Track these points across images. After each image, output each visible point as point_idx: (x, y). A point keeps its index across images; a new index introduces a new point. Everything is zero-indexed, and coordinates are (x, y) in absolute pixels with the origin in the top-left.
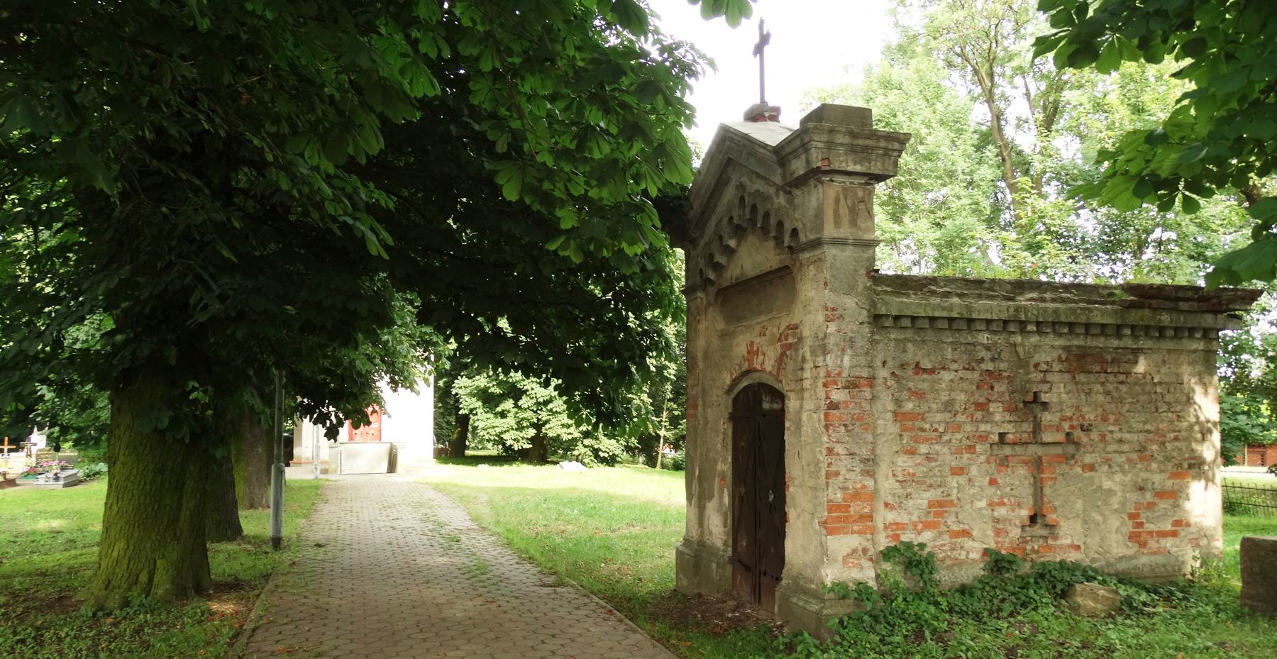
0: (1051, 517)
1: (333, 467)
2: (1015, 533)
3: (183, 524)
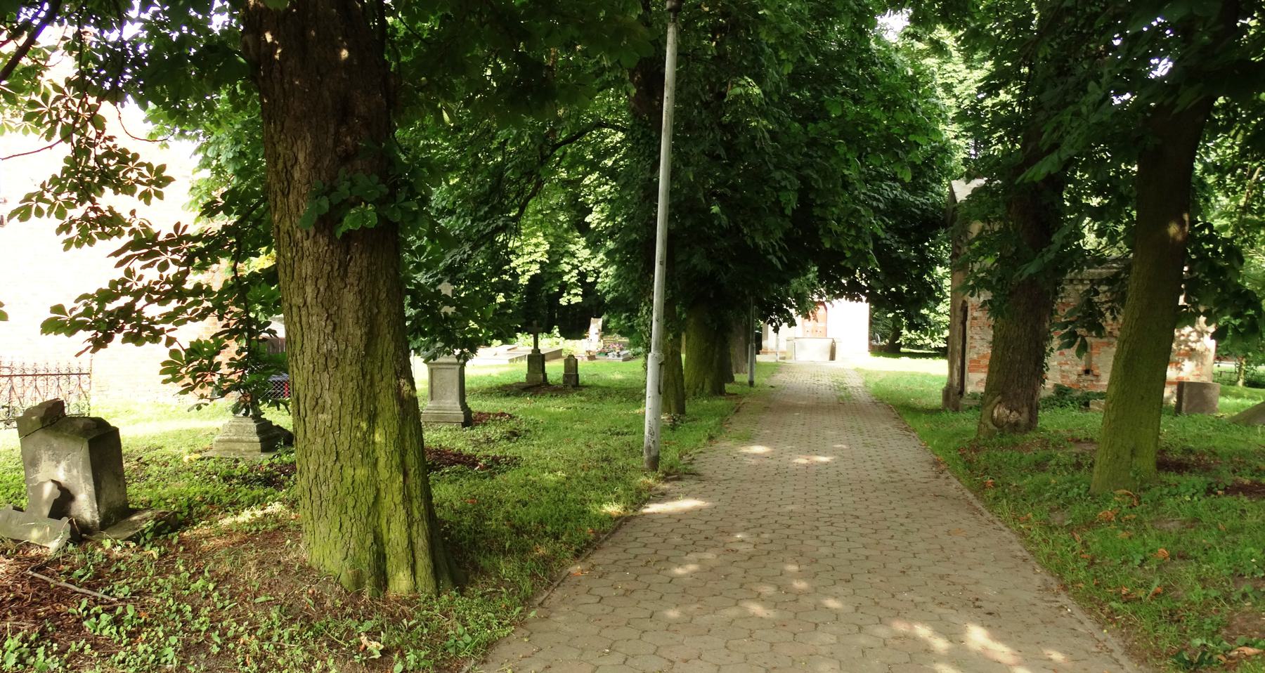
0: (1096, 372)
1: (789, 355)
2: (1074, 377)
3: (715, 364)
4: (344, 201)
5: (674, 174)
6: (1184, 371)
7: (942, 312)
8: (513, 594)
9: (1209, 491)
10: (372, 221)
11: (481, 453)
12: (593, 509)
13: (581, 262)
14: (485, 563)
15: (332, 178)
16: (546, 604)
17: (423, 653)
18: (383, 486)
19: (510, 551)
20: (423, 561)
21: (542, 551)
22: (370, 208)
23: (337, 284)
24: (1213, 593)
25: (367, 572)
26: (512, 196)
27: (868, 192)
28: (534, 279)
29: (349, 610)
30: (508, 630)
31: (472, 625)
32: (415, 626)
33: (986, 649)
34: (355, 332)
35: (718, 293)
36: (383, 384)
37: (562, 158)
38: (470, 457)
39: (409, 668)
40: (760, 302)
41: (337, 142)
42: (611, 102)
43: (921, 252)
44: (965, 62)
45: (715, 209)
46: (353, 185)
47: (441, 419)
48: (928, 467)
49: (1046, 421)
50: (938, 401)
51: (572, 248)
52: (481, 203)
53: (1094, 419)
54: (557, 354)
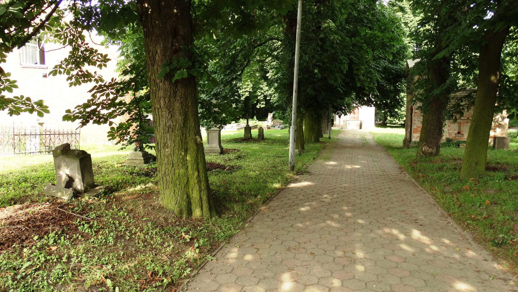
0: (462, 133)
2: (454, 135)
4: (175, 68)
5: (300, 58)
6: (496, 133)
7: (403, 111)
8: (239, 217)
9: (506, 178)
10: (186, 75)
11: (227, 164)
12: (269, 185)
13: (265, 92)
14: (228, 206)
15: (170, 59)
16: (252, 221)
17: (206, 240)
18: (190, 177)
19: (238, 201)
20: (205, 205)
21: (250, 201)
22: (185, 70)
23: (172, 100)
24: (507, 217)
25: (184, 209)
26: (239, 66)
27: (374, 64)
28: (246, 98)
29: (178, 223)
30: (238, 231)
31: (224, 229)
32: (202, 229)
33: (419, 238)
34: (180, 118)
35: (317, 102)
36: (190, 138)
37: (257, 51)
38: (223, 166)
39: (200, 245)
40: (334, 107)
41: (172, 45)
42: (277, 30)
43: (395, 87)
44: (413, 14)
45: (316, 71)
46: (178, 61)
47: (211, 151)
48: (397, 169)
49: (443, 152)
50: (401, 144)
51: (261, 86)
52: (227, 69)
53: (462, 151)
54: (255, 127)
